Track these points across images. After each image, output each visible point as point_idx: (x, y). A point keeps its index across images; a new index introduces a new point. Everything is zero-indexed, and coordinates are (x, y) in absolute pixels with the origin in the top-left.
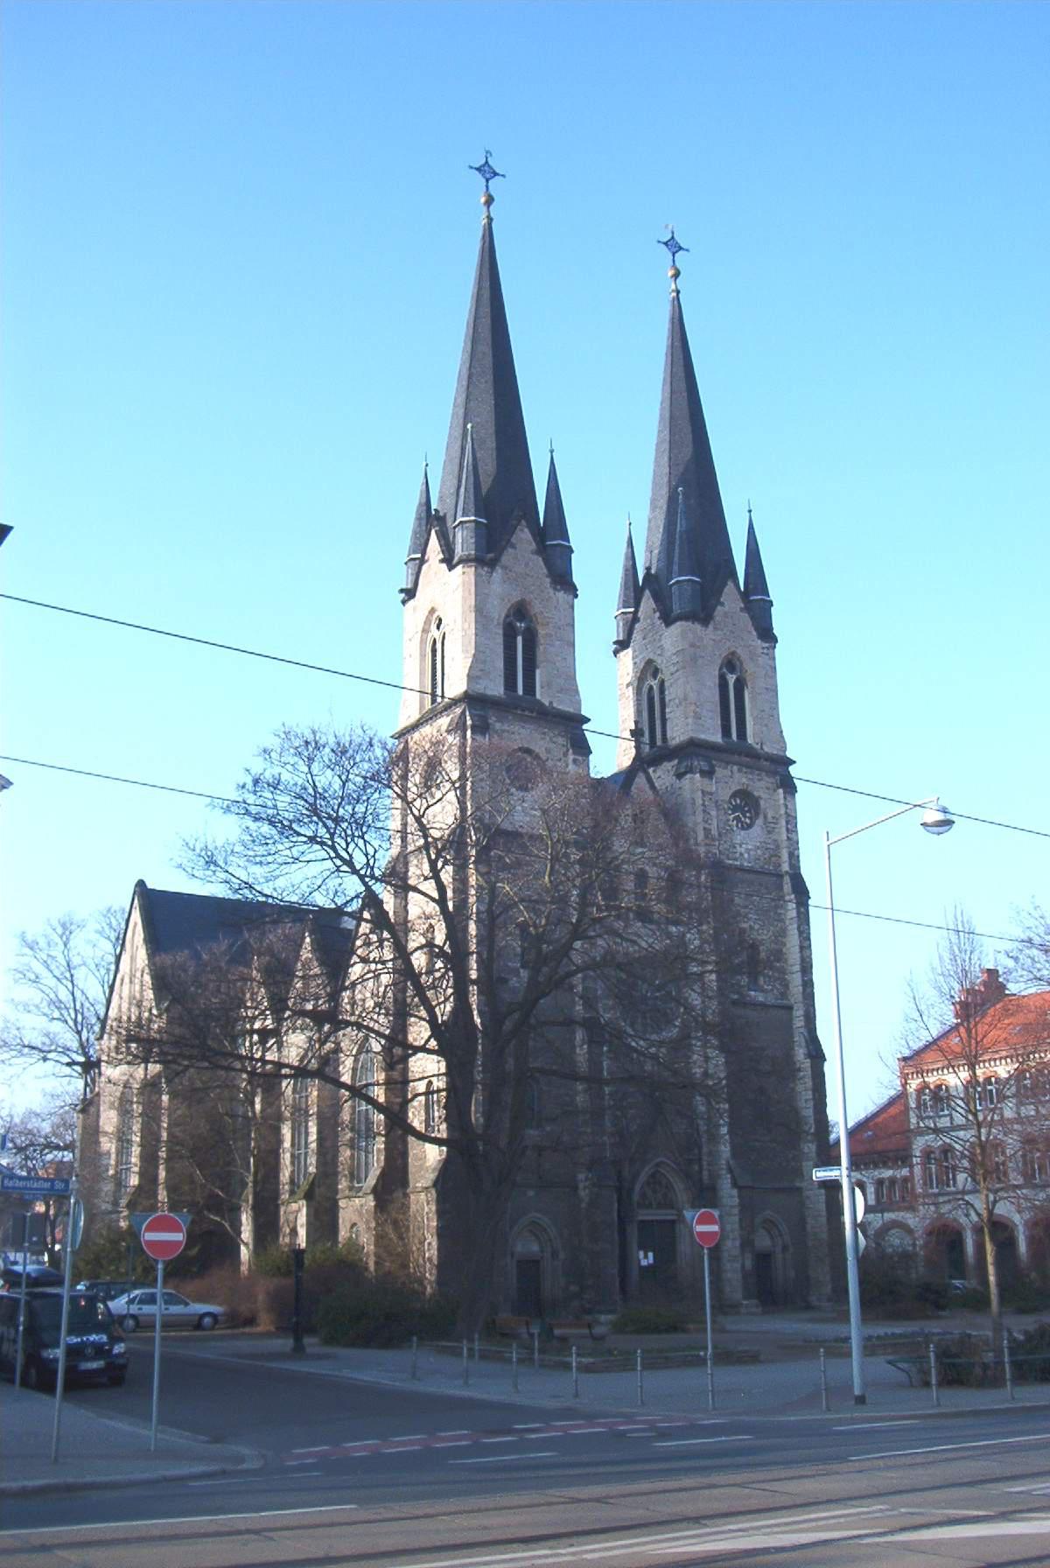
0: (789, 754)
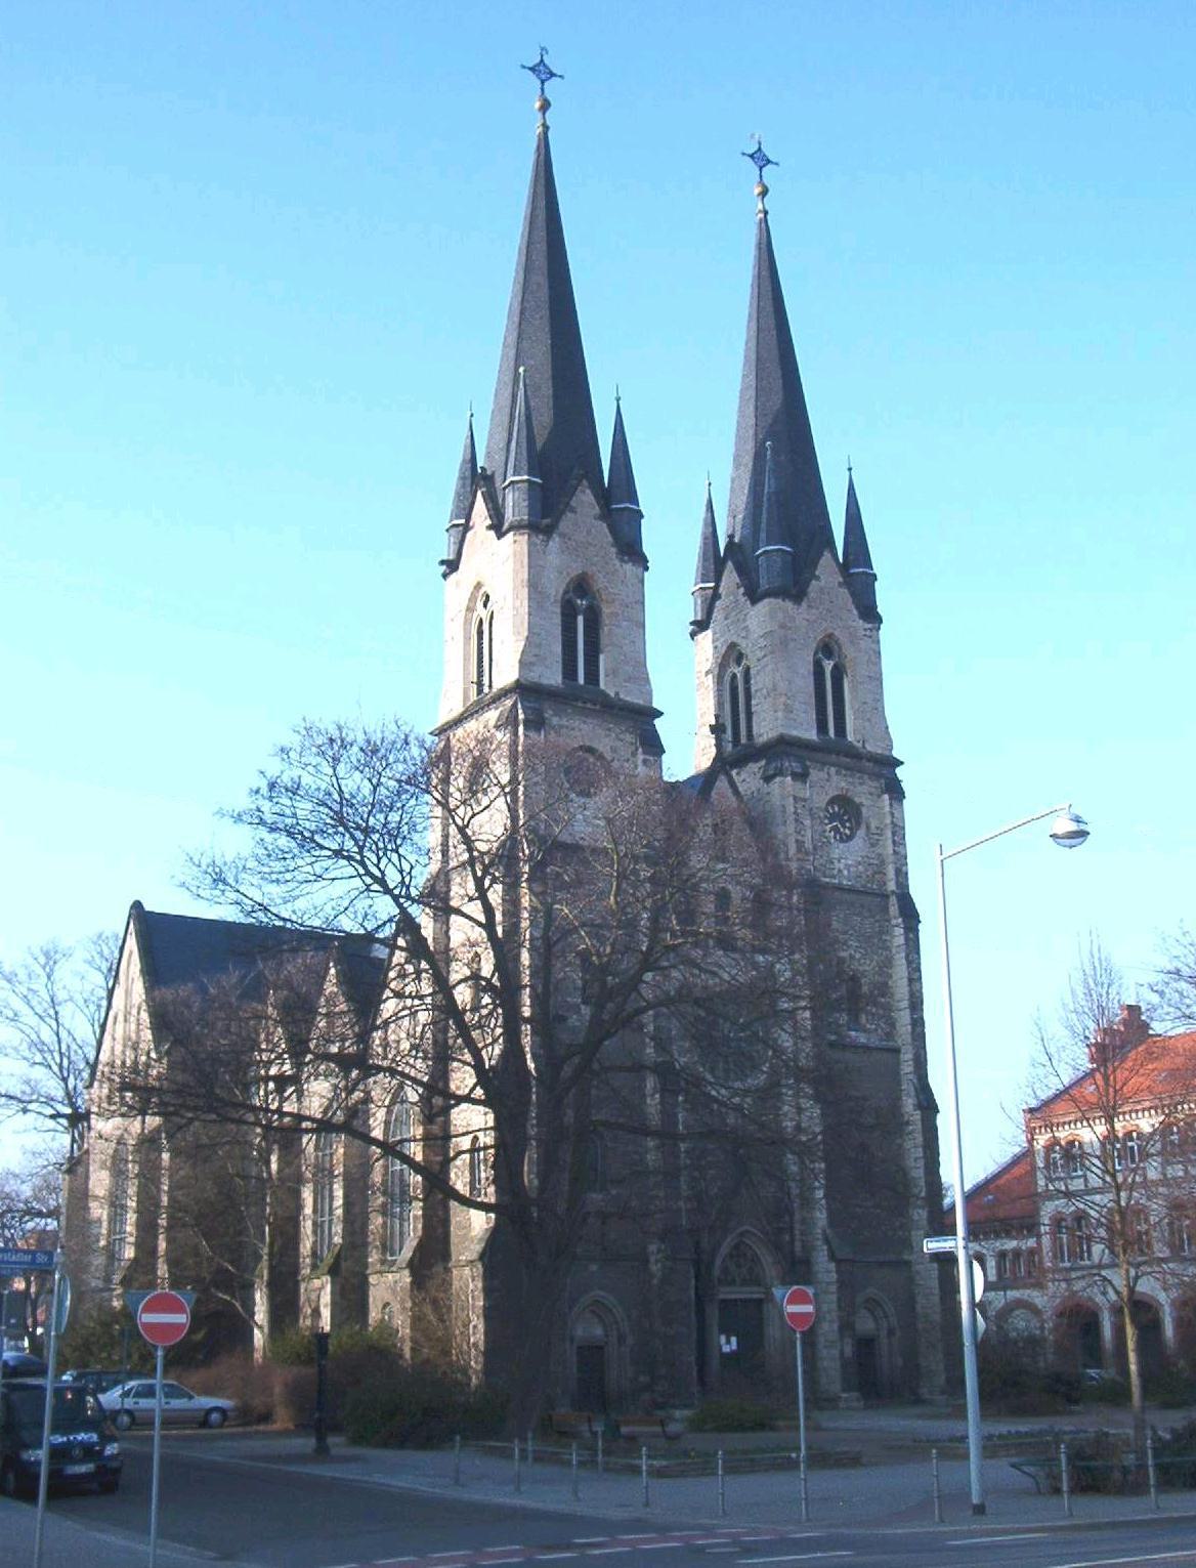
0: (896, 753)
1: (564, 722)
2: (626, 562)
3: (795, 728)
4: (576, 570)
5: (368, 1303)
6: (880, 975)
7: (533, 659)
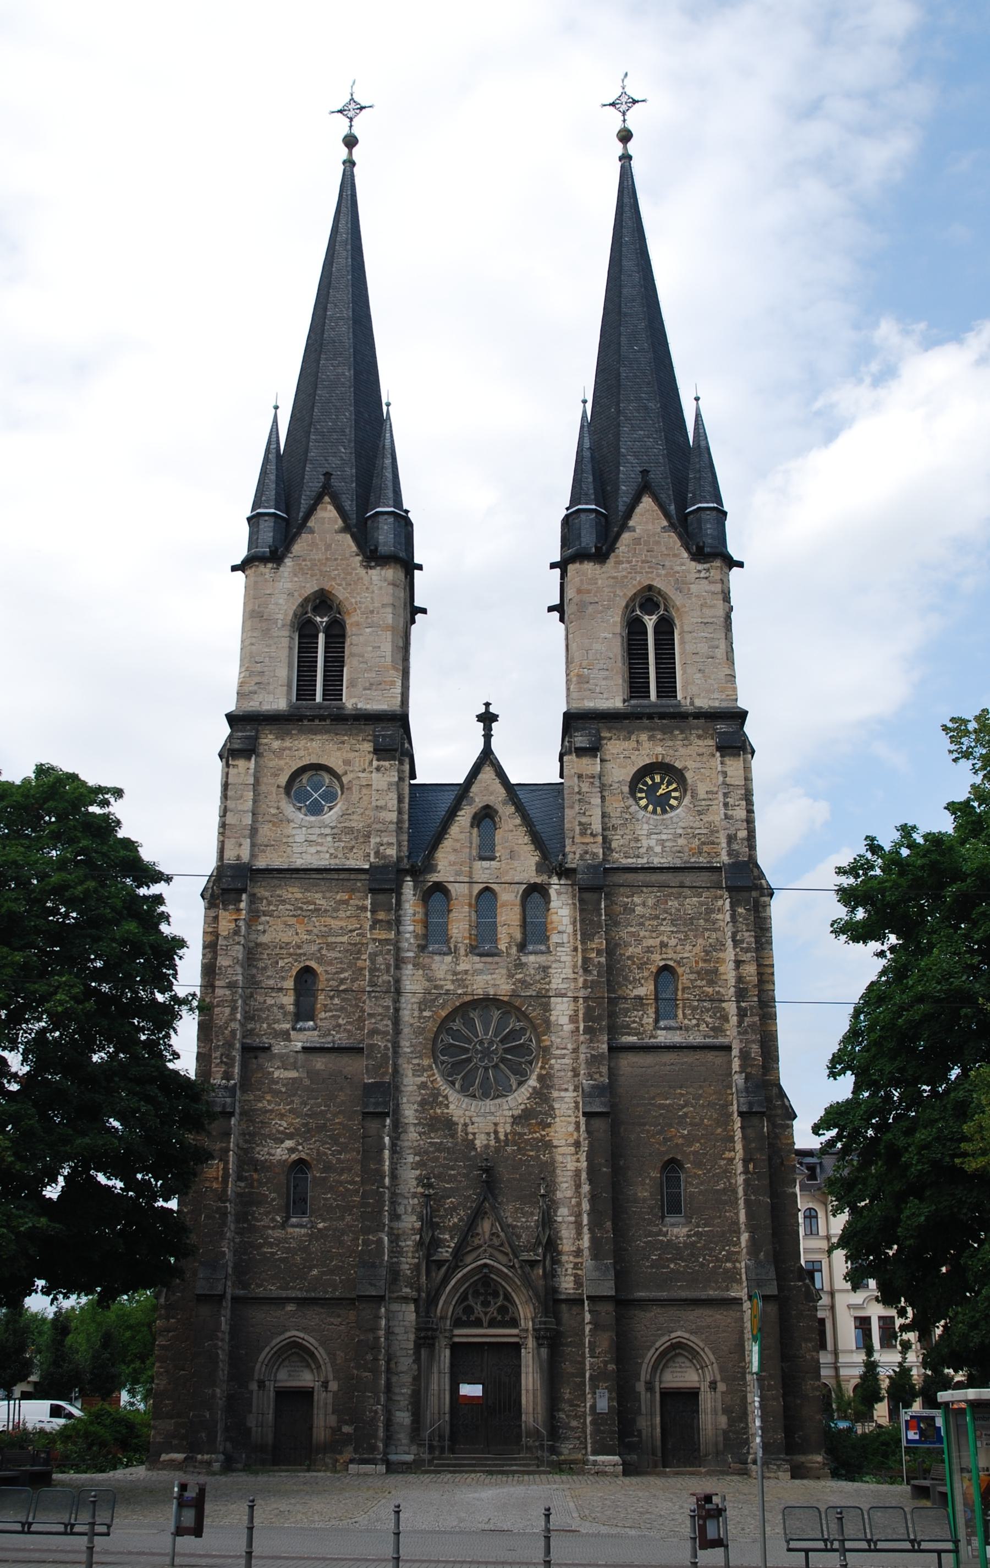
0: (742, 704)
1: (287, 743)
2: (371, 568)
3: (590, 699)
4: (311, 587)
5: (312, 1414)
6: (705, 961)
7: (256, 688)
